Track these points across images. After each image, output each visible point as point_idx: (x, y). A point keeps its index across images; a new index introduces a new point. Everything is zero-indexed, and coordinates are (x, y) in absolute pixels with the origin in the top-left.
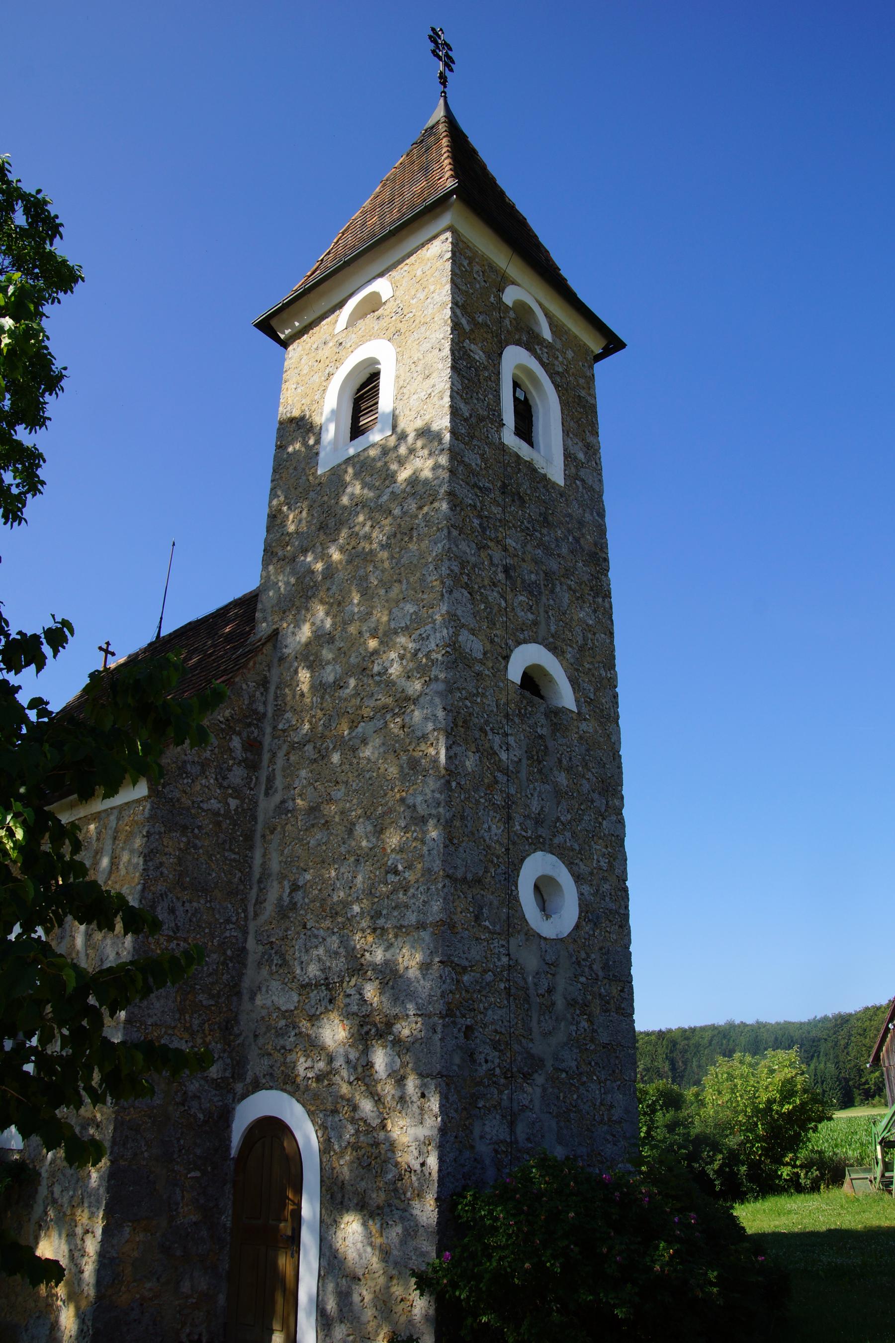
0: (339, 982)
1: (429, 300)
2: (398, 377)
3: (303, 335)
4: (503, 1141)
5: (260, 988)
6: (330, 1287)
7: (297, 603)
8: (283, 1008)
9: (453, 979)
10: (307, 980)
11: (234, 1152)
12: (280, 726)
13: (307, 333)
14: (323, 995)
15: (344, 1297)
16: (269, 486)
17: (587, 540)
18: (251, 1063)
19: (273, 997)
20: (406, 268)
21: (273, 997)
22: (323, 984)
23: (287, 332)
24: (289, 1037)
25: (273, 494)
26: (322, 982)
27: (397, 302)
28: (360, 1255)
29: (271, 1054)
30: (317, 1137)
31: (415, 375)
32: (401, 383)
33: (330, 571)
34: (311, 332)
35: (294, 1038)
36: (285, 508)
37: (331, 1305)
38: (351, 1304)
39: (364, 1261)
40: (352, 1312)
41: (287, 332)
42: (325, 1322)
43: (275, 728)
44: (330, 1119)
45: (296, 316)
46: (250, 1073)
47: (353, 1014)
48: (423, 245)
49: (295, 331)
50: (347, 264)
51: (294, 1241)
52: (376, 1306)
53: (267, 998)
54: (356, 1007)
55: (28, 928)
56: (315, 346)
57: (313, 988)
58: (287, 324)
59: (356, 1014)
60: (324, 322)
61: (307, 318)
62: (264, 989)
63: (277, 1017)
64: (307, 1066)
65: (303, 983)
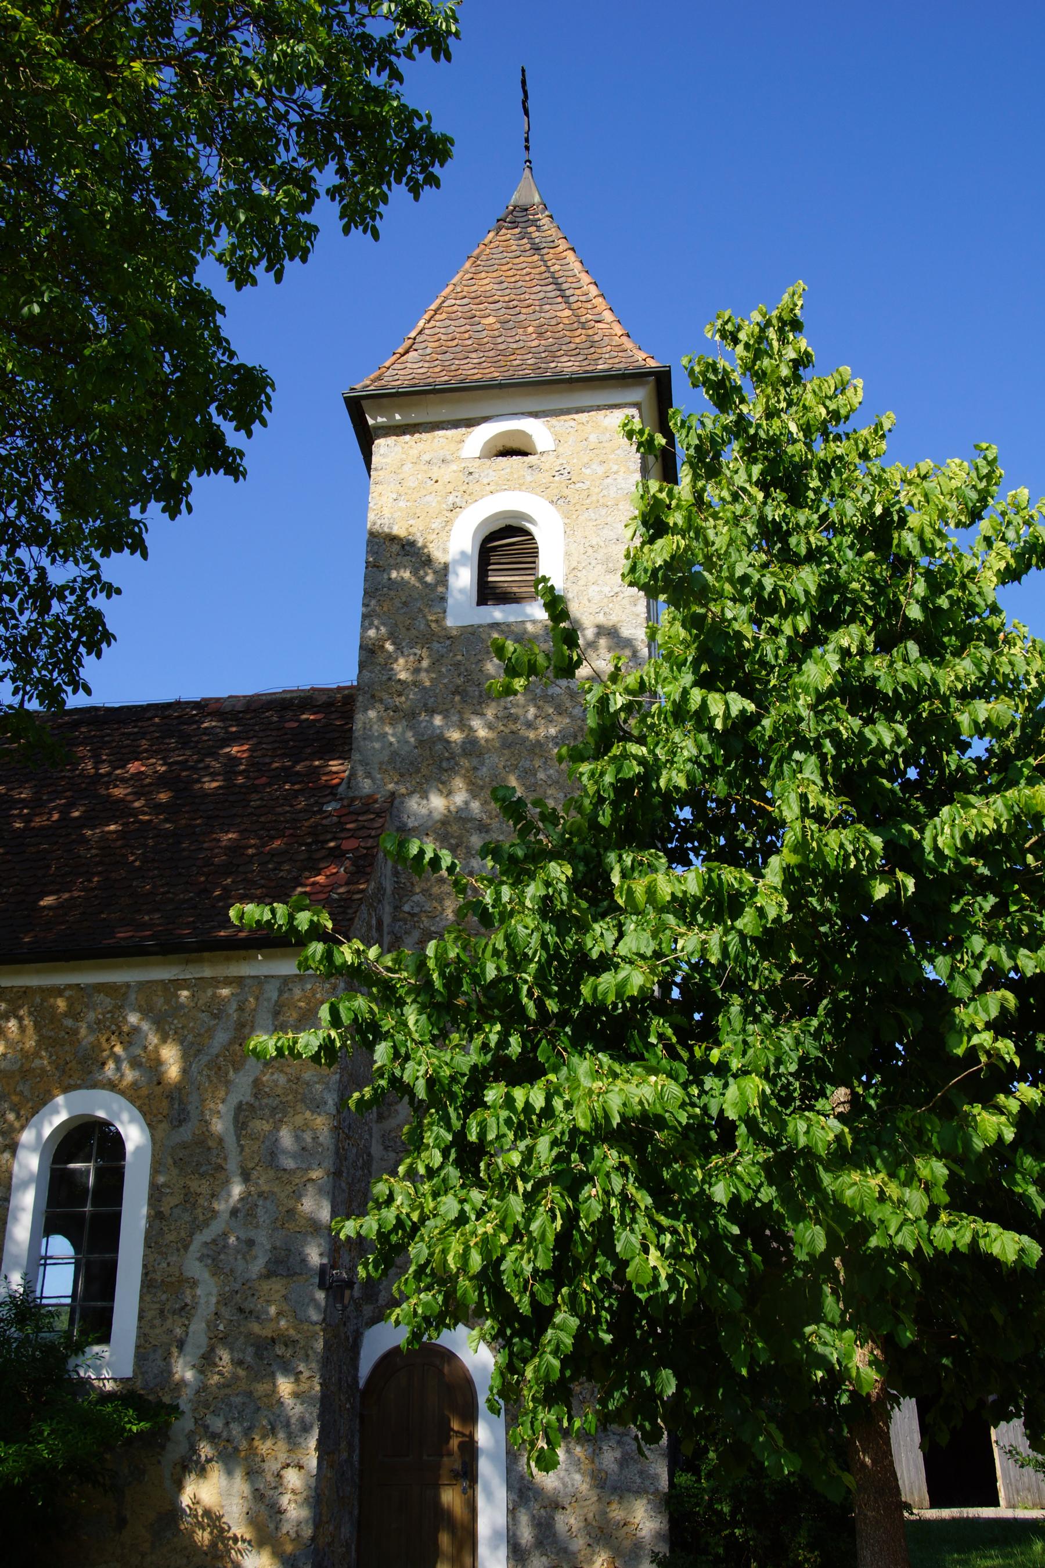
1: (609, 480)
2: (568, 555)
3: (404, 433)
6: (524, 1518)
7: (424, 771)
11: (362, 1383)
12: (406, 908)
13: (412, 434)
15: (545, 1530)
16: (359, 610)
17: (199, 825)
20: (572, 423)
23: (380, 420)
25: (367, 618)
27: (561, 461)
28: (565, 1485)
31: (594, 562)
32: (574, 564)
33: (471, 747)
34: (417, 435)
36: (389, 647)
37: (526, 1535)
38: (555, 1534)
39: (570, 1489)
41: (380, 420)
42: (516, 1552)
43: (397, 908)
45: (399, 409)
46: (383, 1293)
48: (599, 408)
49: (392, 423)
50: (501, 386)
51: (468, 1474)
52: (589, 1534)
55: (901, 924)
56: (426, 457)
58: (380, 411)
60: (441, 433)
61: (414, 417)
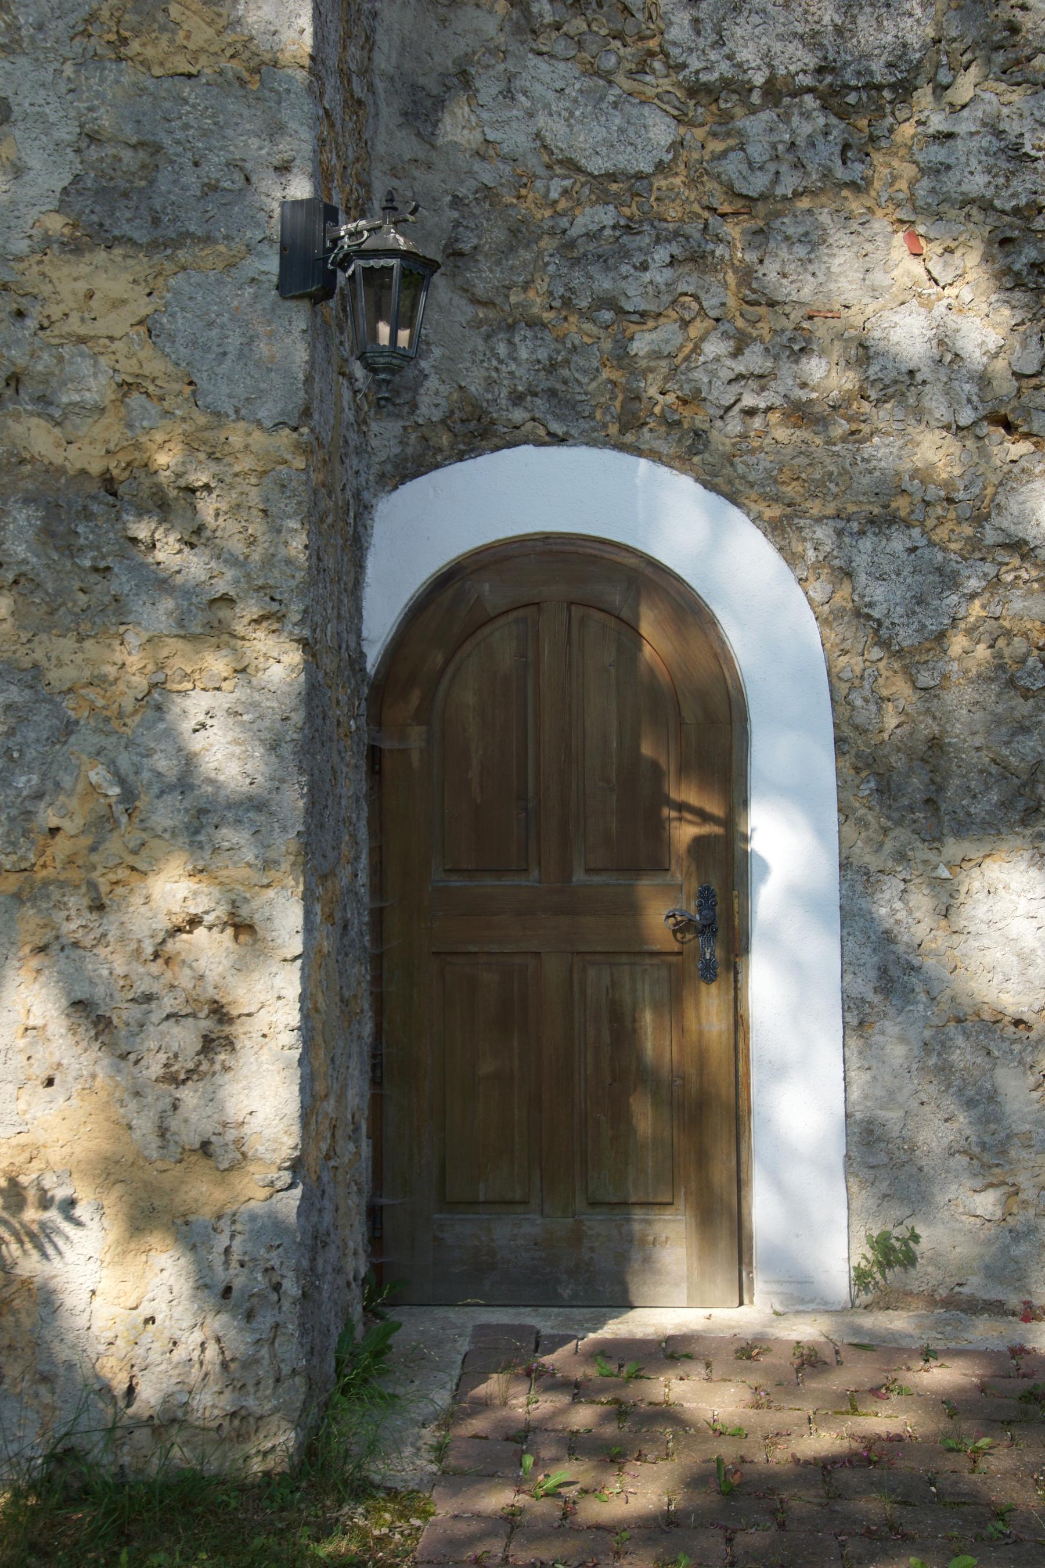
0: (893, 87)
4: (646, 1441)
5: (464, 79)
8: (596, 165)
9: (324, 64)
10: (725, 68)
14: (806, 129)
18: (437, 352)
19: (542, 120)
21: (542, 120)
22: (810, 90)
24: (644, 267)
26: (806, 80)
29: (544, 326)
30: (810, 601)
35: (668, 273)
40: (998, 1120)
44: (866, 544)
46: (433, 383)
47: (967, 201)
53: (508, 121)
54: (981, 179)
57: (756, 98)
59: (986, 206)
62: (488, 88)
63: (565, 192)
64: (741, 368)
65: (704, 77)
